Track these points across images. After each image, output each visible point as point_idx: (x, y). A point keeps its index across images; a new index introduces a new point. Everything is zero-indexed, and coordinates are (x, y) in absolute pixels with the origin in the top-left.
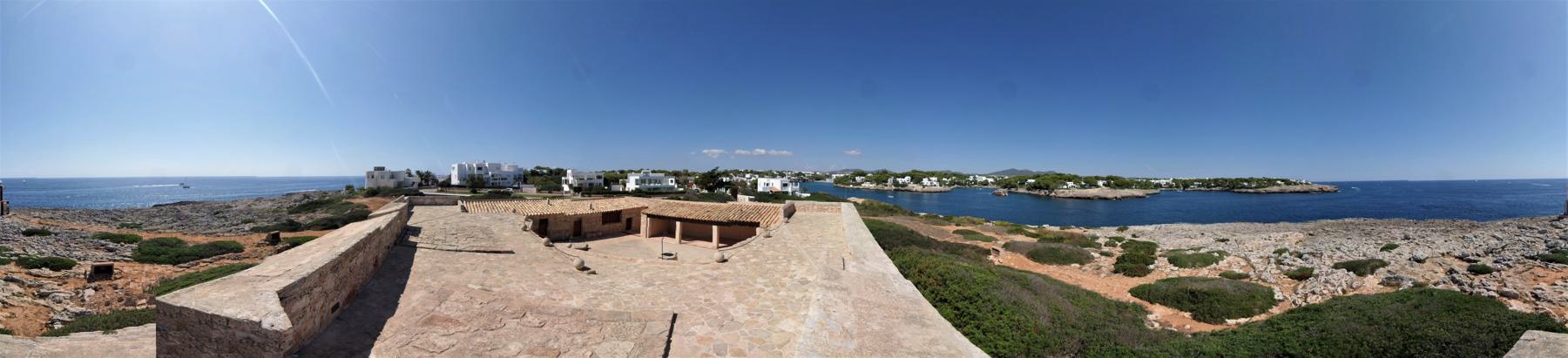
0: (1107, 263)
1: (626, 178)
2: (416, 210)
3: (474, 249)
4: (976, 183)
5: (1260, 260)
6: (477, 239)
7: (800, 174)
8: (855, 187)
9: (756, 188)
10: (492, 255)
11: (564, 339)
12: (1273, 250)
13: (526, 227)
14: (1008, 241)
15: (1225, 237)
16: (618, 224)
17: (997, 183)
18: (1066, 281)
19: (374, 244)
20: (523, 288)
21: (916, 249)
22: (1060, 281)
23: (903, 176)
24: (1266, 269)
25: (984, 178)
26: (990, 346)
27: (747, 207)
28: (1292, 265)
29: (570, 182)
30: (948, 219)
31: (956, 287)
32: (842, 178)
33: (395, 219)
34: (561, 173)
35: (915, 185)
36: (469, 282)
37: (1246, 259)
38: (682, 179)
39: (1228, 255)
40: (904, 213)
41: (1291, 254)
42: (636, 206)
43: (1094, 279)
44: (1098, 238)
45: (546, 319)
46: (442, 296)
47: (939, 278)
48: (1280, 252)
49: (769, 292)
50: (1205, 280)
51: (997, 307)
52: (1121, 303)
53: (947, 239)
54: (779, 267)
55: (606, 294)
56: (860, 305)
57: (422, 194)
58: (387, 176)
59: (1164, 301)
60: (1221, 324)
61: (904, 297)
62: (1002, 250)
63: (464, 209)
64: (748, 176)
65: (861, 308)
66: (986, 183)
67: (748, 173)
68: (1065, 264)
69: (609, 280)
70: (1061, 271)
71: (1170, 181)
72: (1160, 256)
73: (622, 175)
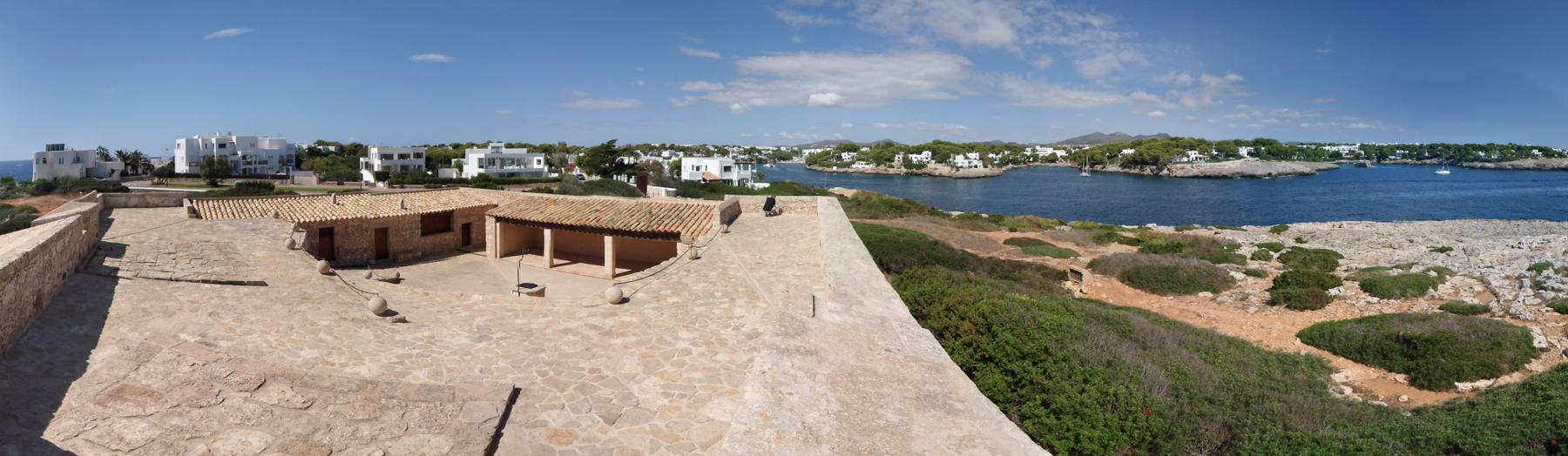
0: (1258, 289)
1: (463, 156)
2: (117, 215)
3: (200, 278)
4: (1036, 158)
5: (1507, 282)
6: (206, 261)
7: (751, 151)
8: (842, 170)
9: (679, 174)
10: (229, 288)
11: (341, 428)
12: (1527, 265)
13: (293, 243)
14: (1097, 256)
15: (1445, 243)
16: (448, 236)
17: (1072, 157)
18: (1191, 322)
19: (34, 270)
20: (268, 342)
21: (941, 271)
22: (1181, 324)
23: (919, 151)
24: (1516, 296)
25: (1050, 151)
26: (1067, 439)
27: (660, 207)
28: (1559, 290)
29: (376, 169)
30: (997, 221)
31: (1007, 335)
32: (819, 155)
33: (71, 226)
34: (358, 150)
35: (939, 166)
36: (182, 331)
37: (1483, 280)
38: (556, 157)
39: (1452, 274)
40: (921, 210)
41: (1557, 272)
42: (477, 204)
43: (1238, 316)
44: (1239, 246)
45: (316, 396)
46: (142, 356)
47: (981, 320)
48: (1538, 268)
49: (701, 355)
50: (1425, 318)
51: (1078, 369)
52: (1286, 356)
53: (994, 254)
54: (717, 311)
55: (418, 356)
56: (862, 379)
57: (126, 190)
58: (69, 160)
59: (1360, 355)
60: (1447, 390)
61: (917, 360)
62: (1086, 273)
63: (194, 213)
64: (666, 154)
65: (865, 384)
66: (1053, 159)
67: (666, 149)
68: (1187, 293)
69: (426, 334)
70: (1181, 306)
71: (1355, 148)
72: (1346, 279)
73: (455, 151)
